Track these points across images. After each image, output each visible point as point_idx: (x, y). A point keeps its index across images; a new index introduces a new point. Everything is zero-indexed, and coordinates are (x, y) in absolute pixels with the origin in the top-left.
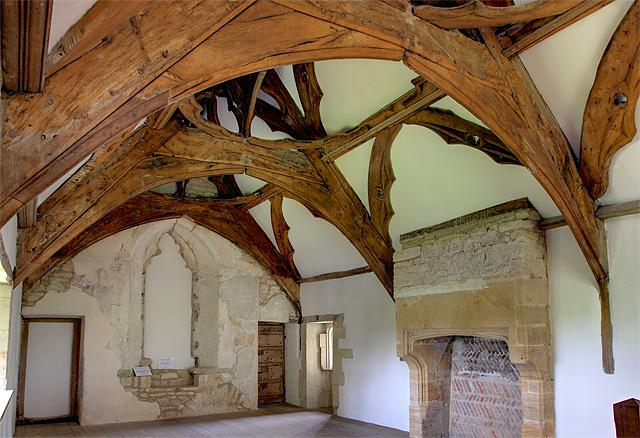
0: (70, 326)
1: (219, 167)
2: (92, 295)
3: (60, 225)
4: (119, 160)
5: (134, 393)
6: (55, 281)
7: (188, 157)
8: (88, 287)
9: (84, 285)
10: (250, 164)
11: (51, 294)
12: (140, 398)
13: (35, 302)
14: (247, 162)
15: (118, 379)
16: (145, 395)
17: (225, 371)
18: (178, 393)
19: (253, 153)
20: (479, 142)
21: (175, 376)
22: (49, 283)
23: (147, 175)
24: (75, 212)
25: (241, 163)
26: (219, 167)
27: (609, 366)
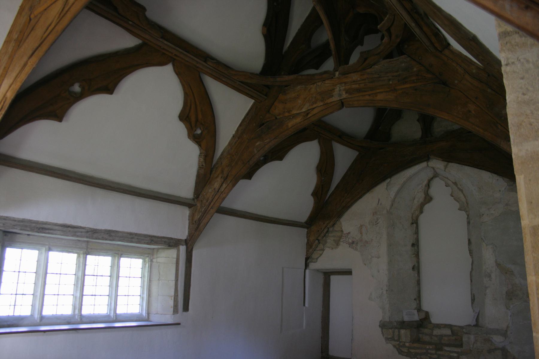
0: (333, 278)
1: (315, 111)
2: (356, 249)
3: (207, 201)
4: (239, 138)
5: (394, 346)
6: (330, 241)
7: (287, 114)
8: (353, 242)
9: (350, 241)
10: (344, 96)
11: (328, 252)
12: (401, 352)
13: (317, 259)
14: (340, 95)
15: (380, 329)
16: (405, 350)
17: (497, 332)
18: (439, 353)
19: (345, 83)
20: (83, 88)
21: (448, 332)
22: (326, 242)
23: (258, 144)
24: (215, 189)
25: (336, 98)
26: (315, 111)
27: (349, 272)
